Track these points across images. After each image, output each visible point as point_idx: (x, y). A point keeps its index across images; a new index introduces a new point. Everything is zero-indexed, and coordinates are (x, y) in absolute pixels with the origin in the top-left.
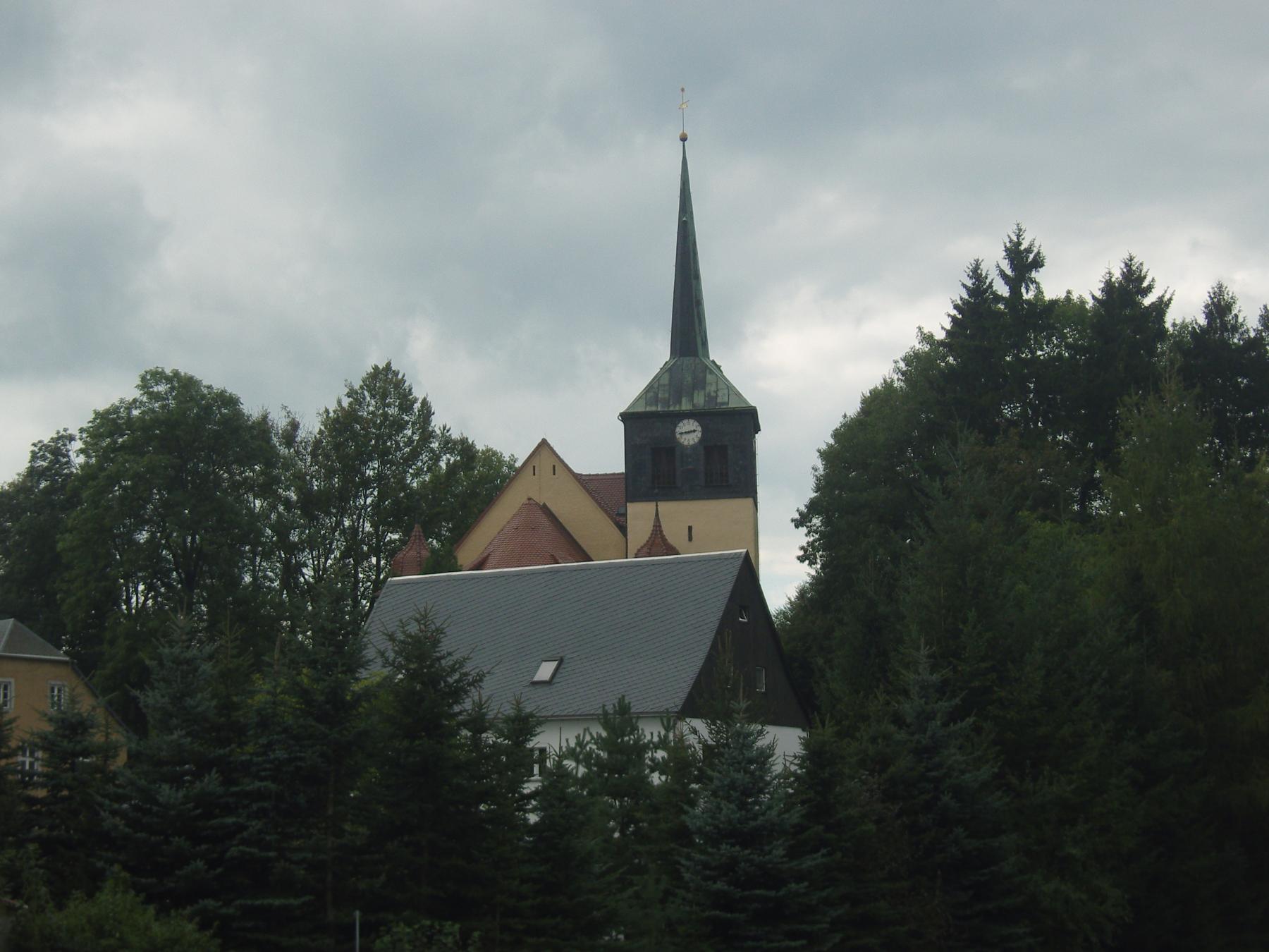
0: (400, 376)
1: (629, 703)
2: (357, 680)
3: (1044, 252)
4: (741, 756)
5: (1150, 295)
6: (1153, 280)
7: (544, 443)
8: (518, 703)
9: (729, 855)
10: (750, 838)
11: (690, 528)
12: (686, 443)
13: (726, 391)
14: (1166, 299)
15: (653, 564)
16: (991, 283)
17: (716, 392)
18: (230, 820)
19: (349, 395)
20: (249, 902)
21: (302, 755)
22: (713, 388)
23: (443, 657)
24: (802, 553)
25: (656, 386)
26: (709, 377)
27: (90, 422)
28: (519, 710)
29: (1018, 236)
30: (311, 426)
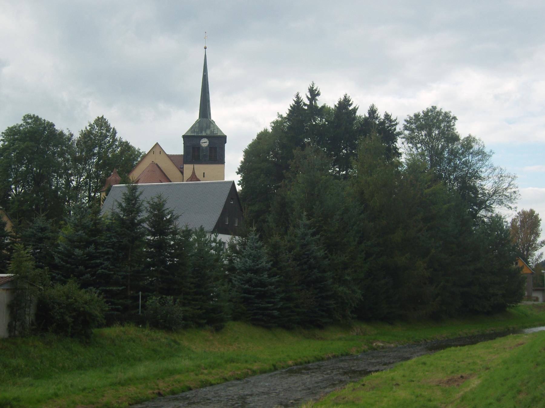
0: (106, 120)
1: (204, 227)
2: (139, 216)
3: (321, 91)
4: (253, 245)
5: (352, 106)
6: (353, 102)
7: (157, 144)
8: (187, 226)
9: (250, 276)
10: (256, 272)
11: (204, 173)
12: (203, 146)
13: (217, 130)
14: (356, 108)
15: (192, 184)
16: (302, 100)
17: (214, 130)
18: (98, 261)
19: (89, 126)
20: (105, 288)
21: (122, 240)
22: (213, 129)
23: (166, 210)
24: (239, 183)
25: (194, 127)
26: (212, 125)
27: (6, 130)
28: (187, 228)
29: (313, 85)
30: (77, 136)
